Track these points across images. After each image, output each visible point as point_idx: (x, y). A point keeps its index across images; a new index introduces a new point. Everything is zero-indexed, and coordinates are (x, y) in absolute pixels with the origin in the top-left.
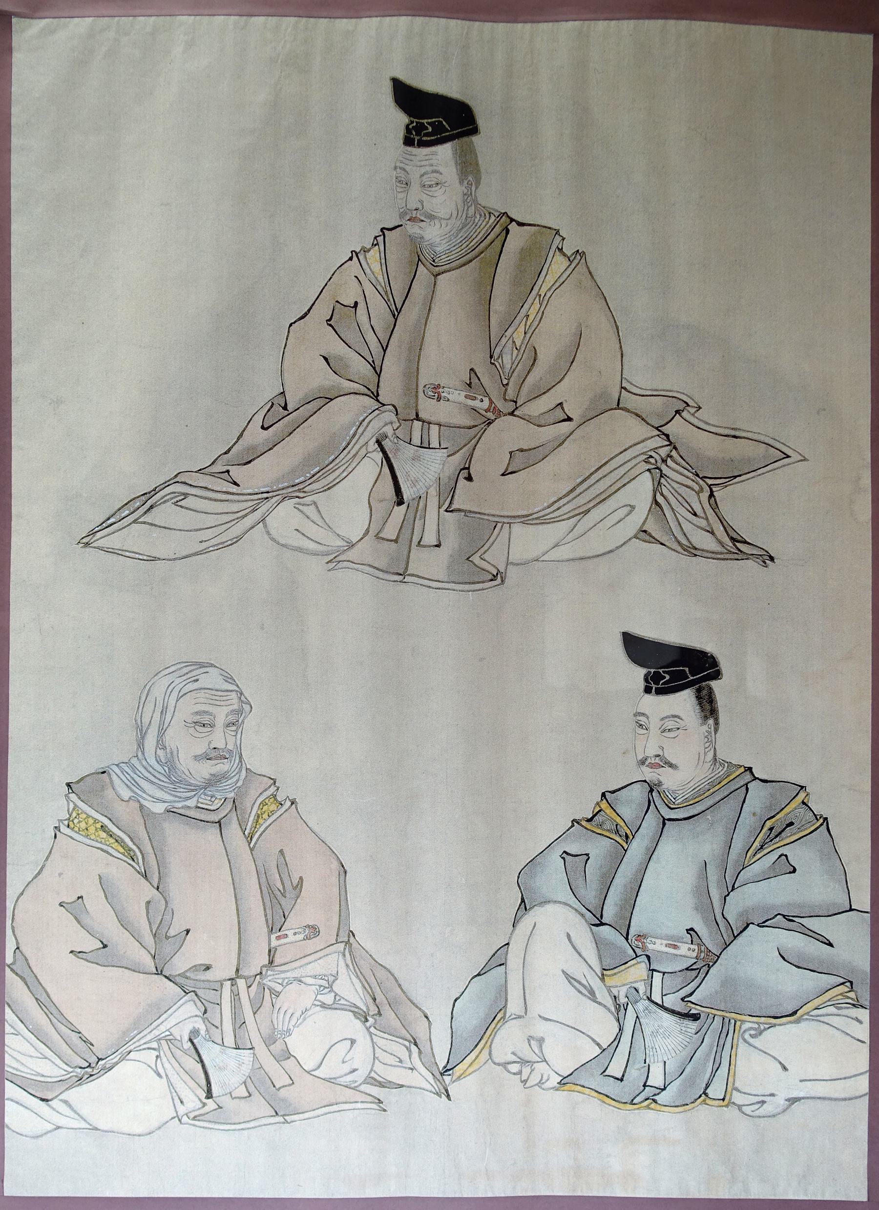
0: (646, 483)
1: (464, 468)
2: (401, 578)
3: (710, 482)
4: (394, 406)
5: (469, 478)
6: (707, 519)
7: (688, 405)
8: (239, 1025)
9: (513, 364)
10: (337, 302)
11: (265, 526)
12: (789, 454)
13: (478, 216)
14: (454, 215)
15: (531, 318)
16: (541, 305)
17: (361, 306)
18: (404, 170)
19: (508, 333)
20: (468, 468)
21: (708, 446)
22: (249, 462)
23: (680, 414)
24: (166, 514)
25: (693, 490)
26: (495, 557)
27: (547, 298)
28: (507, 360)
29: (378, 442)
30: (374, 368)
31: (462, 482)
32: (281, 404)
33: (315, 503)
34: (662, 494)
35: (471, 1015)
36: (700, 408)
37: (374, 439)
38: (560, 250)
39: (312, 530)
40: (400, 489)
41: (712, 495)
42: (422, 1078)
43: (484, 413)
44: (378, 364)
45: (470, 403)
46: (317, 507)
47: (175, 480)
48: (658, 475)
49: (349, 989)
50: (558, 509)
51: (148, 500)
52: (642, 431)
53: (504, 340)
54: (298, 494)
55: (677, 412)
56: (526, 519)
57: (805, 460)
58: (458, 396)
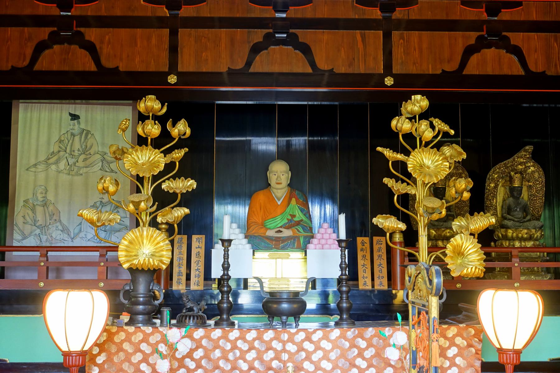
8: (45, 232)
32: (53, 152)
35: (76, 231)
42: (70, 240)
49: (60, 228)
52: (100, 156)
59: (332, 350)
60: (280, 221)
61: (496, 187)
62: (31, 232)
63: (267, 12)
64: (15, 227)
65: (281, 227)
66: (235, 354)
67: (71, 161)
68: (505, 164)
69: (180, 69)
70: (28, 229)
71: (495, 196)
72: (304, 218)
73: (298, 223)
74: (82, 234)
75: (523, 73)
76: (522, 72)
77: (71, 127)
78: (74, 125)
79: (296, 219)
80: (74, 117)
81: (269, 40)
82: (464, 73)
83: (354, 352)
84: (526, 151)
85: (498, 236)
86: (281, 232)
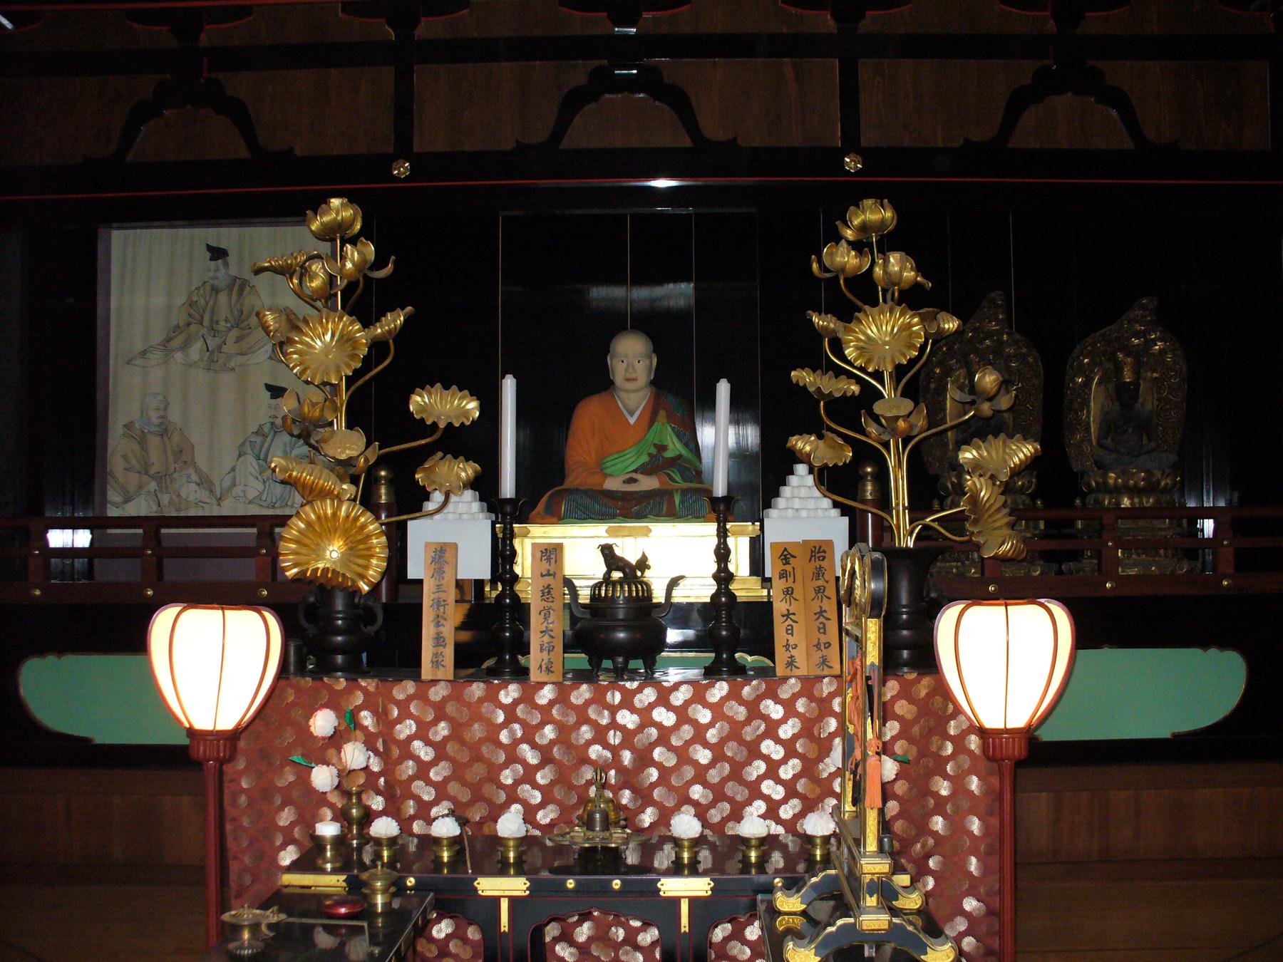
32: (177, 327)
35: (227, 483)
42: (214, 502)
49: (195, 477)
59: (711, 724)
60: (633, 459)
61: (1087, 383)
62: (141, 488)
63: (596, 24)
64: (110, 479)
65: (635, 471)
66: (512, 732)
67: (213, 343)
68: (1103, 335)
69: (417, 148)
70: (133, 479)
71: (1086, 403)
72: (684, 452)
73: (676, 461)
74: (238, 490)
75: (1132, 146)
76: (1129, 144)
77: (211, 274)
78: (217, 270)
79: (669, 454)
80: (218, 253)
81: (603, 83)
82: (1009, 146)
83: (759, 728)
84: (1143, 307)
85: (1089, 485)
86: (635, 481)
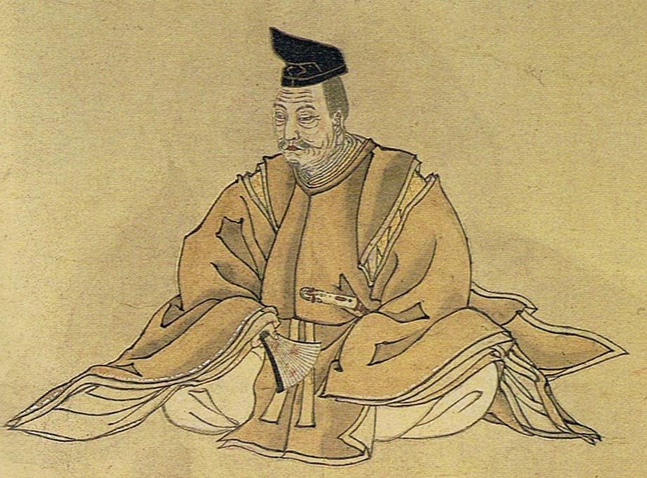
0: (491, 373)
1: (335, 361)
2: (282, 454)
3: (546, 373)
4: (275, 308)
5: (340, 369)
6: (543, 404)
7: (527, 307)
9: (378, 267)
10: (225, 217)
11: (164, 410)
12: (612, 348)
13: (346, 143)
14: (326, 143)
15: (393, 229)
16: (401, 217)
17: (247, 222)
18: (282, 106)
19: (373, 242)
20: (338, 360)
21: (548, 343)
22: (150, 356)
23: (520, 314)
24: (80, 402)
25: (531, 379)
26: (363, 434)
27: (406, 213)
28: (372, 265)
29: (262, 339)
30: (258, 275)
31: (333, 372)
32: (177, 304)
33: (206, 390)
34: (505, 382)
36: (537, 309)
37: (258, 337)
38: (418, 173)
39: (203, 413)
40: (280, 378)
41: (547, 384)
43: (352, 311)
44: (261, 271)
45: (339, 303)
46: (208, 394)
47: (86, 373)
48: (502, 367)
50: (417, 394)
51: (58, 396)
53: (370, 248)
54: (192, 383)
55: (519, 313)
56: (389, 402)
57: (627, 353)
58: (331, 298)
